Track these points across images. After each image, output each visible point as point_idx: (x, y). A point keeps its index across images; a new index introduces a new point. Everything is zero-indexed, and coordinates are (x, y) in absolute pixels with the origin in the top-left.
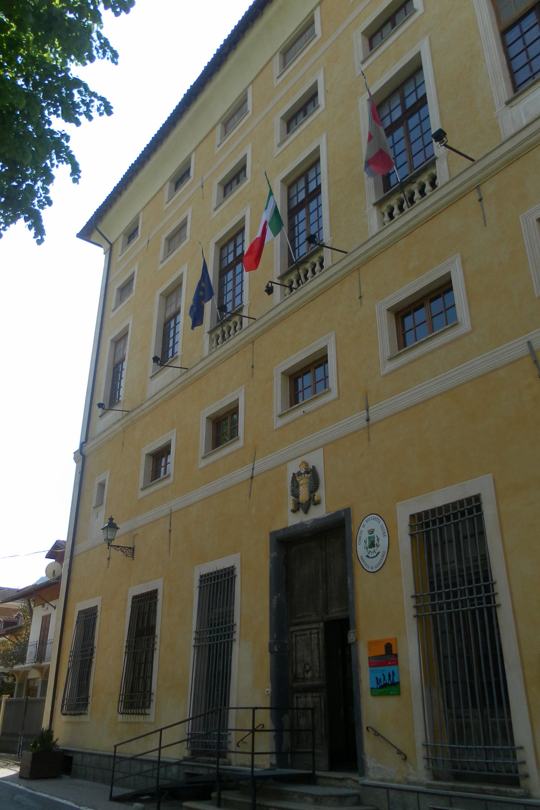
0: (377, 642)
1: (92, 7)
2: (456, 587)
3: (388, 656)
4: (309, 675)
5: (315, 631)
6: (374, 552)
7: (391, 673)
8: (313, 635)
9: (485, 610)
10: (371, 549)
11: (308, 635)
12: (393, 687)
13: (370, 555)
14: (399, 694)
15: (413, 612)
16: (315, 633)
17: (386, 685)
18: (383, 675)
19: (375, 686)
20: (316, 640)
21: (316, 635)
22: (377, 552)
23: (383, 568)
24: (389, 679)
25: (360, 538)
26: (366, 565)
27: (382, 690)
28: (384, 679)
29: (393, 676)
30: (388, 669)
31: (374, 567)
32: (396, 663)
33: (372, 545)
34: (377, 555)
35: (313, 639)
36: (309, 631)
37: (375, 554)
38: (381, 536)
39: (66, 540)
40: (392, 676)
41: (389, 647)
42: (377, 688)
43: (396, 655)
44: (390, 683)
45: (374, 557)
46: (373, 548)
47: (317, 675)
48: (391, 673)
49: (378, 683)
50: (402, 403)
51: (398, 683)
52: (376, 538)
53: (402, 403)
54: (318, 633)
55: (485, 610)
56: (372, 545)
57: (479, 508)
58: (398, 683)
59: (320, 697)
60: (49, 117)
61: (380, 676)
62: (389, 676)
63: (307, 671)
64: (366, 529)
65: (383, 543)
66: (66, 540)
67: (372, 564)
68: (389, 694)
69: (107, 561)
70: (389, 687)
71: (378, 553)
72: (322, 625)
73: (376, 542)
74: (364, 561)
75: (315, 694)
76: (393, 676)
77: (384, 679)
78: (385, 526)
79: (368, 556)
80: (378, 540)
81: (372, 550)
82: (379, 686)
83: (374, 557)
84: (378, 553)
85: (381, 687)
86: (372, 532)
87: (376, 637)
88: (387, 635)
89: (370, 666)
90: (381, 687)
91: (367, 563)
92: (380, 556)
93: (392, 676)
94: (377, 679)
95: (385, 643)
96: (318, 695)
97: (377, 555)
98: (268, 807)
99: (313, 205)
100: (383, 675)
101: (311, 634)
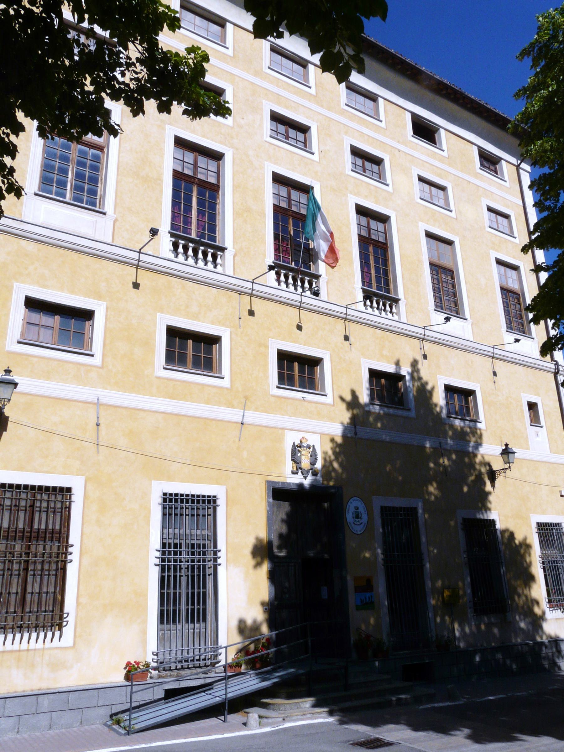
1: (561, 264)
2: (165, 562)
3: (366, 586)
5: (293, 564)
6: (359, 521)
13: (356, 523)
15: (536, 530)
25: (348, 510)
30: (368, 595)
34: (360, 524)
37: (359, 523)
39: (255, 19)
57: (386, 507)
60: (547, 611)
62: (369, 598)
64: (353, 505)
65: (365, 517)
66: (255, 19)
67: (359, 529)
69: (101, 421)
70: (368, 605)
73: (360, 516)
80: (361, 515)
81: (357, 520)
92: (362, 525)
97: (360, 524)
99: (362, 169)
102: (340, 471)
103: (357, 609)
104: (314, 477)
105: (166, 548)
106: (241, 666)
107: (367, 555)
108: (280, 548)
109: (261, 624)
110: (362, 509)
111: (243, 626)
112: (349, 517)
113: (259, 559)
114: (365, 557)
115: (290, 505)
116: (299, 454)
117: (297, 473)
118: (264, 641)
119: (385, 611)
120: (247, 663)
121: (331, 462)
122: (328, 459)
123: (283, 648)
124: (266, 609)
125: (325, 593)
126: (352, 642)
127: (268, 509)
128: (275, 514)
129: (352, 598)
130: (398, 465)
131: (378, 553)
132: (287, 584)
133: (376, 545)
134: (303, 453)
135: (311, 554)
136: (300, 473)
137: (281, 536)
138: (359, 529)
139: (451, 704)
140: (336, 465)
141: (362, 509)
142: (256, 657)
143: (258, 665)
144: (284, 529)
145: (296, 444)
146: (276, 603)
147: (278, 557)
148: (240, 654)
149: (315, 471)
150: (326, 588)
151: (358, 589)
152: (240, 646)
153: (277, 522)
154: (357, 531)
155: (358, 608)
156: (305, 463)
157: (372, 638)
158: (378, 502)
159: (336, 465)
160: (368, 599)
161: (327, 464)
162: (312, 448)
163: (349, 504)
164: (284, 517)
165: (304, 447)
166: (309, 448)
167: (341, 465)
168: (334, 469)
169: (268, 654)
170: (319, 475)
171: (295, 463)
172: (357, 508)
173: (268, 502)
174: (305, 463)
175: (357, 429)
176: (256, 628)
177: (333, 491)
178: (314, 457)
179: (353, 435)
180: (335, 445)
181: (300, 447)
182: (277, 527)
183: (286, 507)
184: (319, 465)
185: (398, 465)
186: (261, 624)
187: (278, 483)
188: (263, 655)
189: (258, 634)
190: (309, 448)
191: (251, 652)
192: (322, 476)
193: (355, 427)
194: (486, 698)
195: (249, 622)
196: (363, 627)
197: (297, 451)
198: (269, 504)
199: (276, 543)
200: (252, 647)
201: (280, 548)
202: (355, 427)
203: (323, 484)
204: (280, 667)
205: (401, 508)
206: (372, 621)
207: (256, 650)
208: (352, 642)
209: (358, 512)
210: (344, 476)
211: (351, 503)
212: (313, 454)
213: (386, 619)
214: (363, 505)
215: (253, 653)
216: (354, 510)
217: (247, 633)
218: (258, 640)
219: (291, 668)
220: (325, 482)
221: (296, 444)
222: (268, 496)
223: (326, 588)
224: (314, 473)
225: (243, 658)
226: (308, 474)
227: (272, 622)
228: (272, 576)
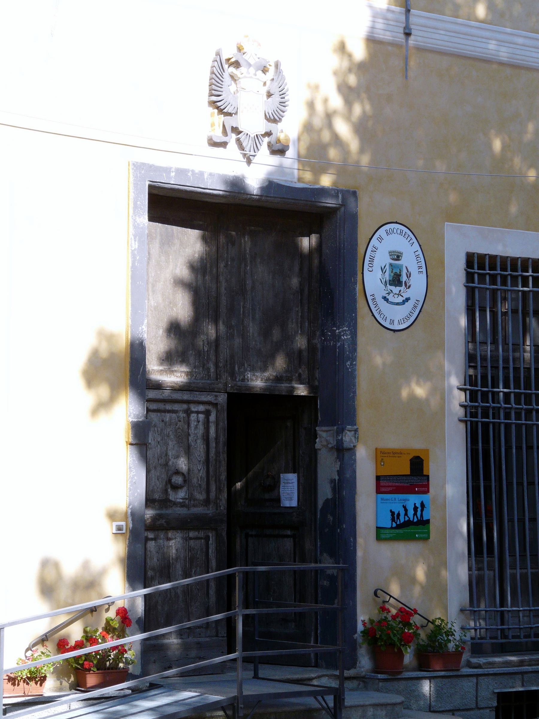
0: (396, 453)
3: (415, 475)
4: (181, 494)
5: (201, 408)
6: (399, 295)
7: (418, 505)
8: (193, 417)
9: (513, 427)
10: (393, 288)
11: (182, 415)
12: (421, 526)
13: (390, 298)
14: (426, 538)
16: (198, 413)
17: (408, 524)
18: (404, 507)
19: (387, 522)
20: (201, 427)
21: (201, 416)
22: (406, 296)
23: (412, 327)
24: (415, 514)
25: (372, 260)
26: (380, 313)
27: (401, 531)
28: (406, 514)
29: (422, 511)
30: (413, 500)
31: (396, 322)
32: (425, 489)
33: (396, 280)
34: (404, 302)
35: (193, 424)
36: (185, 406)
37: (400, 300)
38: (414, 270)
40: (419, 510)
41: (418, 465)
42: (392, 528)
43: (428, 476)
44: (416, 520)
45: (397, 304)
46: (398, 288)
47: (200, 496)
48: (418, 505)
49: (393, 520)
50: (478, 44)
51: (428, 521)
52: (404, 272)
53: (478, 44)
54: (207, 413)
55: (513, 427)
56: (396, 280)
58: (428, 521)
59: (207, 538)
61: (398, 508)
62: (415, 509)
63: (176, 488)
64: (383, 249)
67: (397, 316)
68: (410, 538)
70: (411, 528)
71: (408, 299)
72: (222, 398)
73: (404, 278)
74: (376, 305)
75: (192, 534)
76: (422, 511)
77: (406, 514)
78: (421, 256)
79: (385, 298)
80: (409, 275)
81: (396, 290)
82: (394, 525)
83: (397, 304)
84: (408, 299)
85: (399, 527)
86: (397, 256)
87: (392, 443)
88: (416, 444)
89: (379, 491)
90: (399, 527)
91: (383, 311)
92: (409, 305)
93: (419, 510)
94: (393, 513)
95: (411, 457)
96: (202, 534)
97: (404, 302)
98: (213, 717)
100: (404, 507)
101: (188, 412)
102: (354, 144)
103: (379, 538)
104: (275, 160)
105: (531, 404)
106: (43, 679)
107: (420, 391)
108: (169, 359)
109: (103, 572)
110: (411, 261)
111: (51, 576)
112: (373, 280)
113: (104, 391)
114: (413, 397)
115: (204, 239)
116: (233, 88)
117: (224, 145)
118: (112, 614)
119: (459, 544)
120: (61, 672)
121: (329, 117)
122: (319, 108)
123: (163, 636)
124: (119, 528)
125: (290, 490)
126: (360, 627)
127: (136, 246)
128: (153, 262)
129: (369, 509)
130: (529, 136)
131: (450, 388)
132: (182, 464)
133: (447, 366)
134: (243, 83)
135: (258, 382)
136: (232, 145)
137: (174, 328)
138: (397, 316)
139: (513, 714)
140: (343, 128)
141: (411, 261)
142: (87, 656)
143: (91, 680)
144: (181, 308)
145: (224, 57)
146: (149, 513)
147: (158, 386)
148: (40, 648)
149: (278, 141)
150: (292, 477)
151: (384, 485)
152: (42, 627)
153: (160, 286)
154: (392, 322)
155: (381, 534)
156: (252, 122)
157: (416, 620)
158: (461, 241)
159: (343, 128)
160: (411, 513)
161: (318, 122)
162: (272, 70)
163: (374, 241)
164: (182, 271)
165: (250, 65)
166: (265, 70)
167: (360, 128)
168: (336, 139)
169: (121, 650)
170: (291, 153)
171: (221, 111)
172: (397, 256)
173: (136, 227)
174: (252, 122)
175: (412, 19)
176: (89, 584)
177: (330, 202)
178: (276, 98)
179: (401, 37)
180: (346, 64)
181: (237, 64)
182: (160, 299)
183: (188, 243)
184: (290, 129)
185: (529, 136)
186: (103, 572)
187: (167, 170)
188: (105, 654)
189: (93, 594)
190: (265, 70)
191: (72, 643)
192: (299, 157)
193: (408, 11)
194: (519, 659)
195: (70, 569)
196: (395, 589)
197: (226, 76)
198: (138, 234)
199: (156, 344)
200: (76, 632)
201: (169, 359)
202: (408, 11)
203: (300, 180)
204: (153, 686)
205: (525, 261)
206: (420, 573)
207: (89, 639)
208: (360, 627)
209: (400, 268)
210: (365, 160)
211: (380, 239)
212: (275, 90)
213: (459, 571)
214: (416, 246)
215: (79, 645)
216: (388, 260)
217: (64, 593)
218: (93, 610)
219: (185, 690)
220: (308, 176)
221: (224, 57)
222: (135, 207)
223: (292, 477)
224: (277, 147)
225: (49, 659)
226: (257, 148)
227: (137, 570)
228: (141, 437)
